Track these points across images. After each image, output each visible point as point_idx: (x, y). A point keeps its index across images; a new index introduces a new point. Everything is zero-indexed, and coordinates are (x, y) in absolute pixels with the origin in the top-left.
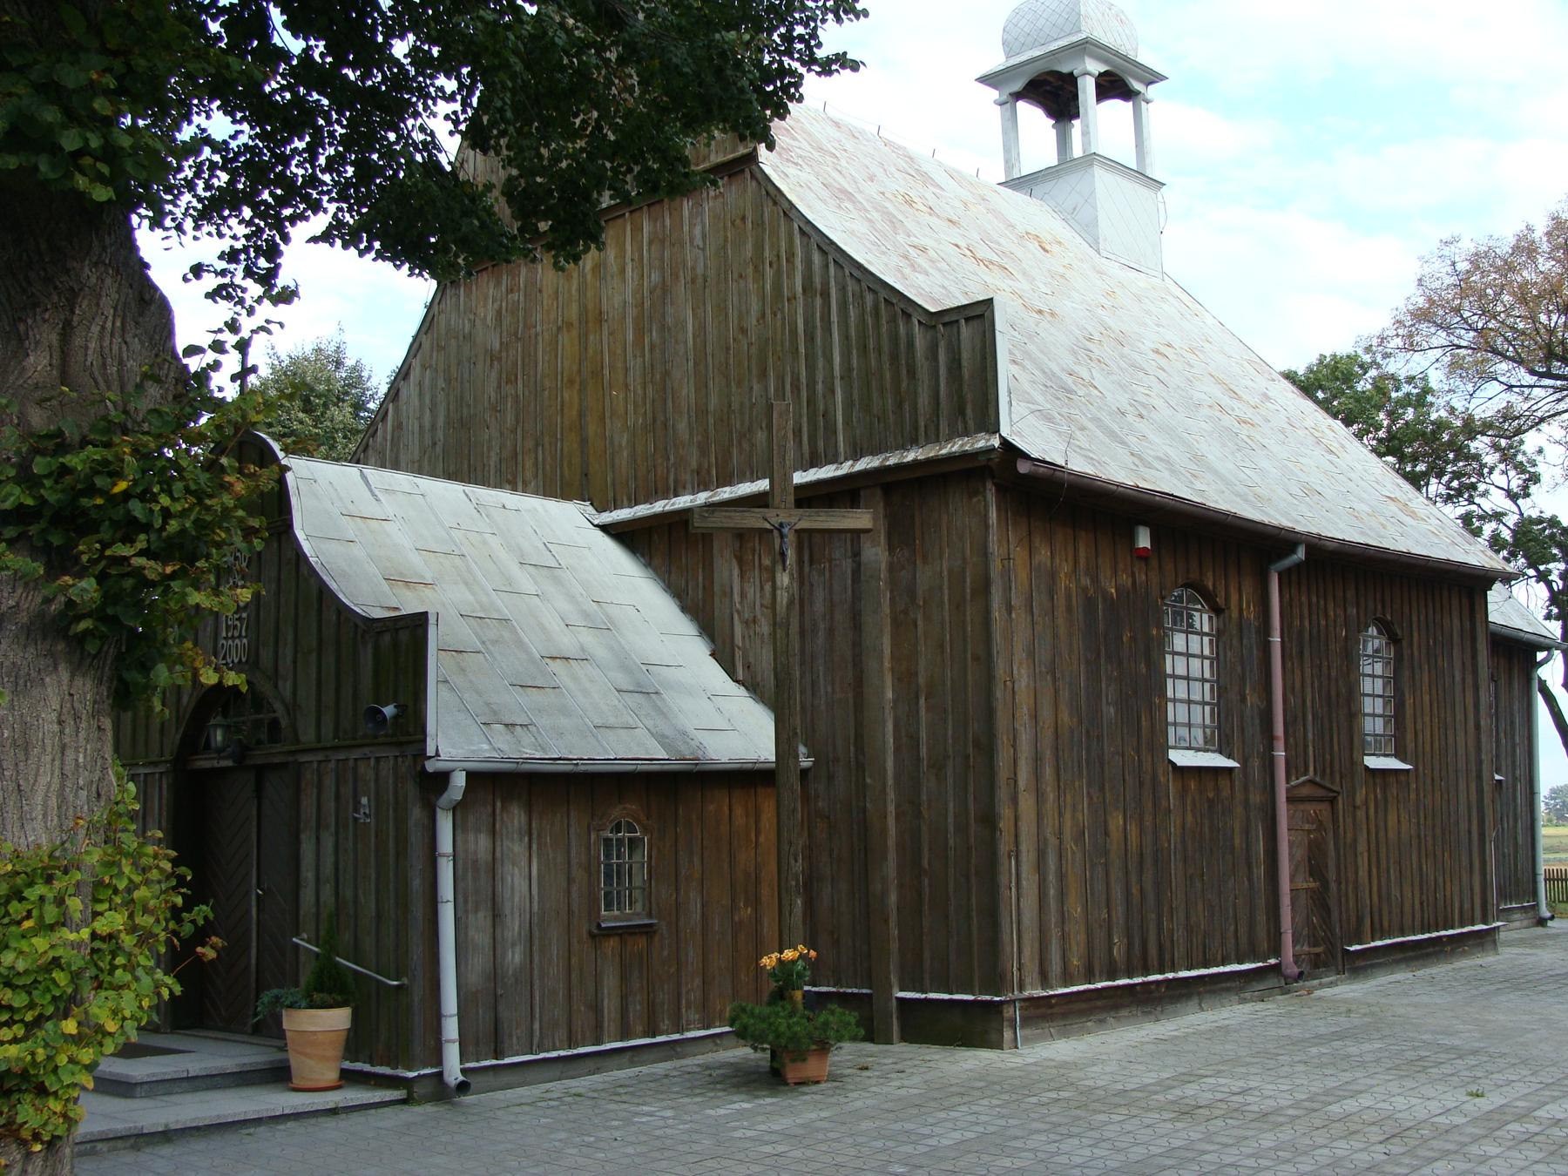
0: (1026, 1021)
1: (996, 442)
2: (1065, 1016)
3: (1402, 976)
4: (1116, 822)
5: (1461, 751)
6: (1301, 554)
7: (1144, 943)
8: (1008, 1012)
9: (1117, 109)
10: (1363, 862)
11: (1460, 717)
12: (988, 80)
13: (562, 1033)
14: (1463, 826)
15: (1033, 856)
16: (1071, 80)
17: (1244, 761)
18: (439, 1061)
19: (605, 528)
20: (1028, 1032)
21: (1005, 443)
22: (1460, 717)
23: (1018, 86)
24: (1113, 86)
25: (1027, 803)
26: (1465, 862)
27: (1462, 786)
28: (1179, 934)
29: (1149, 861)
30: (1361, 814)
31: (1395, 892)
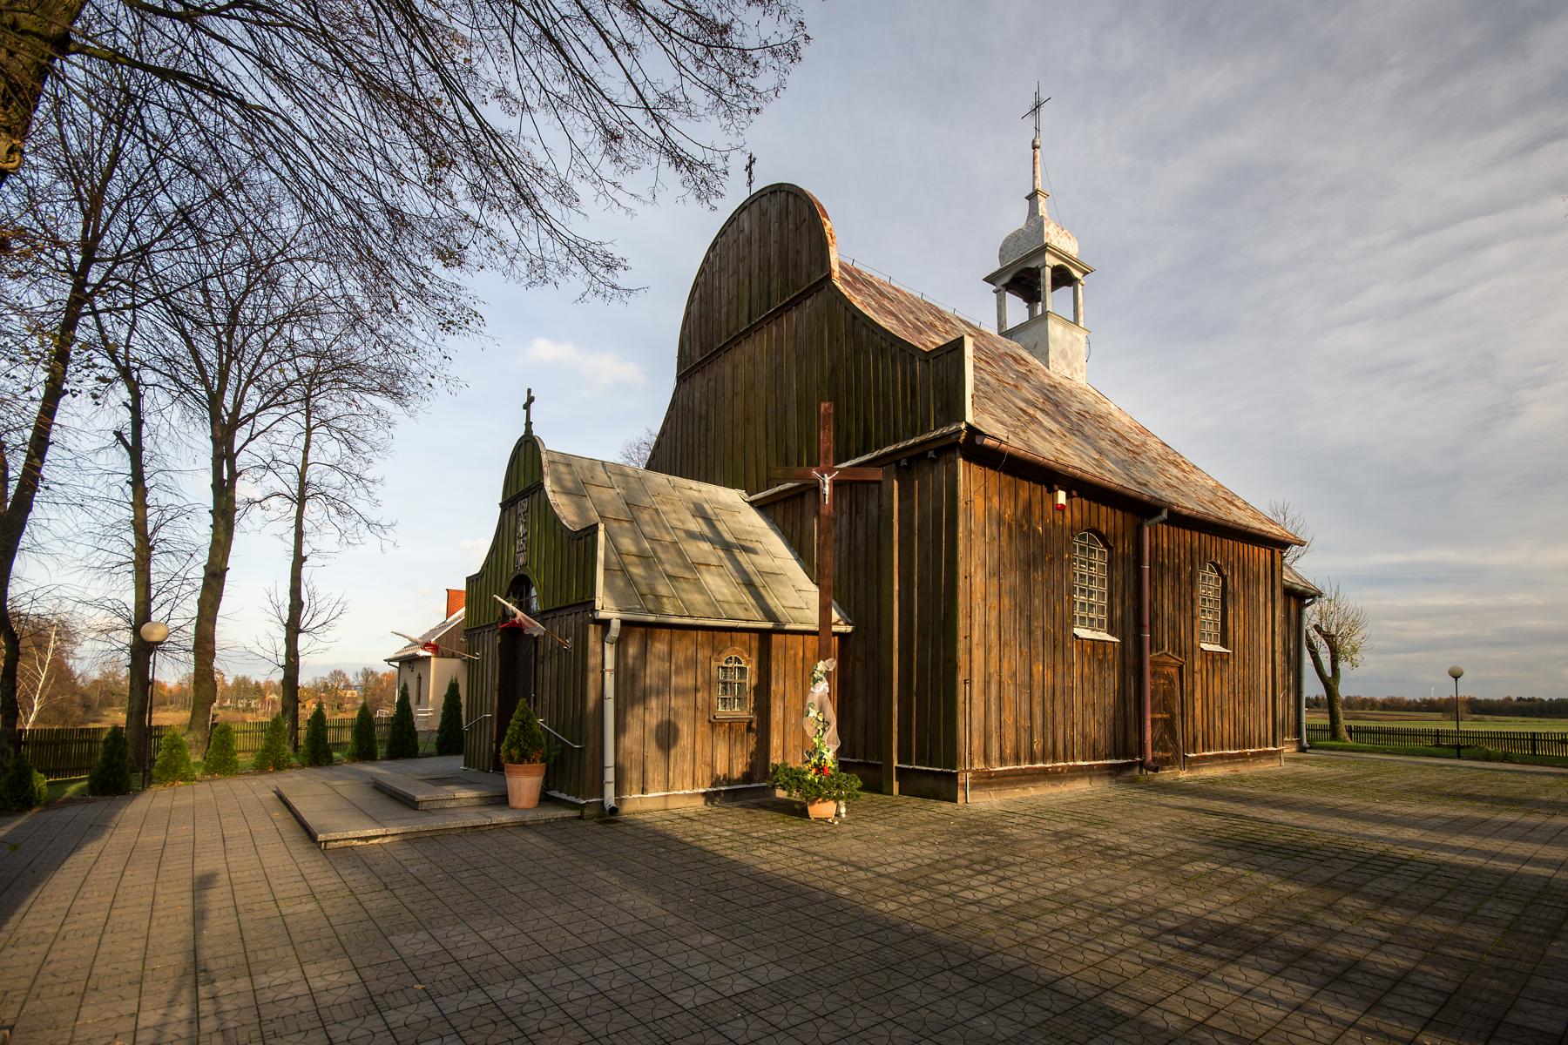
0: (973, 787)
1: (963, 426)
2: (999, 784)
3: (1408, 697)
4: (1038, 669)
5: (1262, 645)
6: (1165, 515)
7: (1054, 743)
8: (432, 748)
9: (1066, 291)
10: (1198, 705)
11: (1262, 624)
12: (990, 279)
13: (689, 780)
14: (1262, 688)
15: (982, 685)
16: (1036, 273)
17: (1123, 639)
18: (602, 796)
19: (751, 503)
20: (976, 793)
21: (969, 427)
22: (1262, 624)
23: (1006, 280)
24: (1063, 278)
25: (978, 654)
26: (1263, 709)
27: (1262, 665)
28: (1078, 738)
29: (1058, 693)
30: (1197, 677)
31: (1218, 724)
